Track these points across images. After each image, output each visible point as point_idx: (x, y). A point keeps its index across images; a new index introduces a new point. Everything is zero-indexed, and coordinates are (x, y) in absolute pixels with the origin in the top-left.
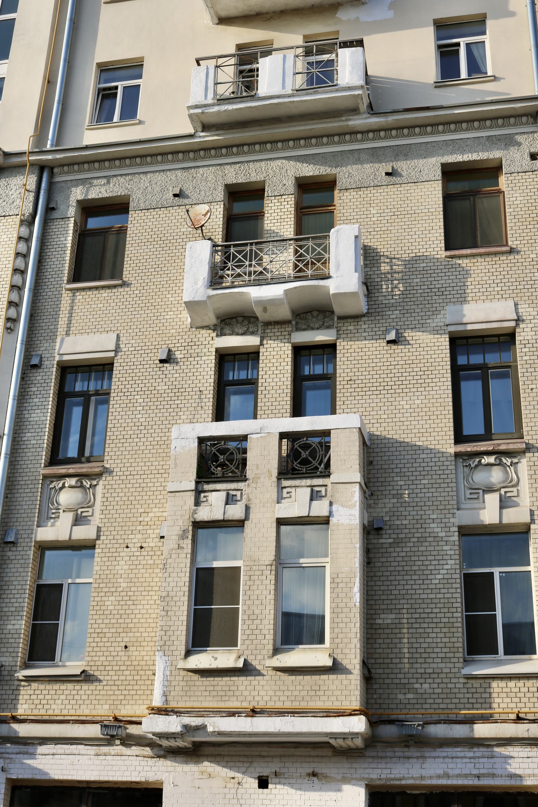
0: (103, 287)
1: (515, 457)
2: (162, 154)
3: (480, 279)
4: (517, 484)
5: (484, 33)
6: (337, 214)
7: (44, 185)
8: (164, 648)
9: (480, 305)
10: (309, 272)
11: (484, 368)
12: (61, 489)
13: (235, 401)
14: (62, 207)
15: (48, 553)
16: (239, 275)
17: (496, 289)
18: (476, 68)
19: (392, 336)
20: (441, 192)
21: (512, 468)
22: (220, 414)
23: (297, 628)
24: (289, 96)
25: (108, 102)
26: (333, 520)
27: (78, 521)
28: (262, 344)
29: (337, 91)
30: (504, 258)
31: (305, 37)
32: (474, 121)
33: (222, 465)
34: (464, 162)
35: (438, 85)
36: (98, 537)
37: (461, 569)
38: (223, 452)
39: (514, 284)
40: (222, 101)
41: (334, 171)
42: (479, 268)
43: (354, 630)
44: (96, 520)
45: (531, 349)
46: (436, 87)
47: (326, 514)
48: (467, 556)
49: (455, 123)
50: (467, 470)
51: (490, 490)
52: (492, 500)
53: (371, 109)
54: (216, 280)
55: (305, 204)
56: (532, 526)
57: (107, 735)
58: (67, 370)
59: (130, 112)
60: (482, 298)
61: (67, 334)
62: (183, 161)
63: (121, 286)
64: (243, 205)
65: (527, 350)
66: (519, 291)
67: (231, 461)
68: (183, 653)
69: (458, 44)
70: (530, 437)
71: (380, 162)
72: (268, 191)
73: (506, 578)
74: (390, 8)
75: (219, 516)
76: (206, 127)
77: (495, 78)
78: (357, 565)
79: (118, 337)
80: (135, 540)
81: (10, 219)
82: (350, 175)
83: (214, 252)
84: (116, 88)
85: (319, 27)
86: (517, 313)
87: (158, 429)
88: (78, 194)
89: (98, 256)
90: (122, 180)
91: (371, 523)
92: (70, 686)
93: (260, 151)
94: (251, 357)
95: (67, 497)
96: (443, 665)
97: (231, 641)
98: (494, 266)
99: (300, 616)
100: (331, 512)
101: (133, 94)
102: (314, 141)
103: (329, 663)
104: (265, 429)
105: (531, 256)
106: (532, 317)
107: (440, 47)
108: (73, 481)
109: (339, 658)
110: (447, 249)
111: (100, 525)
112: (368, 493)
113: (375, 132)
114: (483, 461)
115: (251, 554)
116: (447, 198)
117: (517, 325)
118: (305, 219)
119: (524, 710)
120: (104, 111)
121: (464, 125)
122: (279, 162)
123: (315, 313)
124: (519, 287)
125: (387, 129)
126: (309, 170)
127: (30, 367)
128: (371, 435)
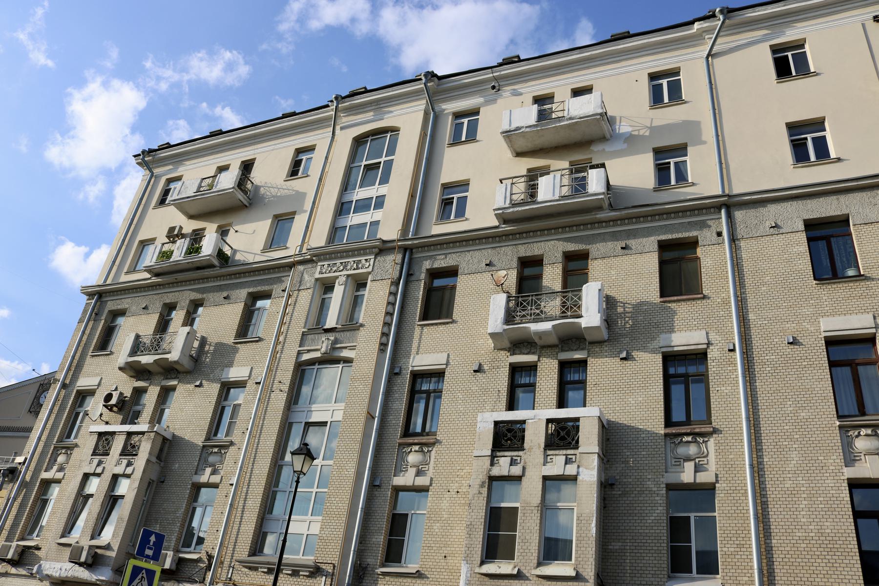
0: (440, 324)
2: (479, 239)
4: (707, 456)
6: (590, 275)
7: (406, 260)
8: (467, 559)
9: (683, 334)
10: (569, 313)
11: (686, 376)
13: (572, 395)
14: (417, 274)
15: (401, 493)
16: (524, 316)
18: (682, 177)
19: (624, 355)
22: (511, 405)
23: (554, 548)
24: (557, 200)
25: (448, 207)
26: (580, 478)
27: (419, 473)
28: (539, 360)
29: (588, 196)
31: (570, 162)
33: (510, 439)
35: (656, 190)
36: (431, 484)
37: (668, 513)
38: (509, 431)
40: (514, 205)
41: (588, 247)
42: (683, 310)
43: (591, 552)
44: (430, 473)
47: (575, 473)
48: (670, 504)
49: (667, 214)
50: (673, 445)
51: (688, 459)
52: (689, 466)
53: (611, 207)
54: (509, 318)
55: (569, 269)
56: (717, 485)
58: (417, 376)
59: (461, 213)
61: (417, 354)
62: (492, 243)
63: (451, 323)
64: (529, 271)
67: (515, 437)
68: (479, 562)
69: (669, 163)
71: (618, 240)
72: (545, 261)
73: (699, 520)
74: (624, 142)
75: (505, 473)
76: (505, 222)
77: (693, 184)
78: (595, 508)
79: (448, 355)
80: (454, 487)
81: (385, 282)
82: (598, 250)
83: (508, 301)
84: (453, 198)
85: (579, 156)
87: (469, 415)
88: (427, 265)
89: (438, 305)
90: (454, 255)
91: (607, 480)
92: (409, 580)
93: (541, 236)
94: (532, 368)
95: (413, 458)
96: (653, 579)
97: (510, 556)
99: (557, 540)
100: (578, 473)
101: (463, 201)
103: (573, 574)
104: (537, 417)
107: (792, 141)
108: (417, 448)
109: (580, 571)
110: (662, 296)
112: (605, 460)
113: (614, 221)
115: (526, 498)
116: (662, 263)
117: (708, 347)
118: (570, 278)
120: (444, 215)
121: (673, 215)
122: (552, 242)
123: (574, 340)
125: (622, 219)
126: (571, 247)
127: (394, 374)
128: (609, 421)
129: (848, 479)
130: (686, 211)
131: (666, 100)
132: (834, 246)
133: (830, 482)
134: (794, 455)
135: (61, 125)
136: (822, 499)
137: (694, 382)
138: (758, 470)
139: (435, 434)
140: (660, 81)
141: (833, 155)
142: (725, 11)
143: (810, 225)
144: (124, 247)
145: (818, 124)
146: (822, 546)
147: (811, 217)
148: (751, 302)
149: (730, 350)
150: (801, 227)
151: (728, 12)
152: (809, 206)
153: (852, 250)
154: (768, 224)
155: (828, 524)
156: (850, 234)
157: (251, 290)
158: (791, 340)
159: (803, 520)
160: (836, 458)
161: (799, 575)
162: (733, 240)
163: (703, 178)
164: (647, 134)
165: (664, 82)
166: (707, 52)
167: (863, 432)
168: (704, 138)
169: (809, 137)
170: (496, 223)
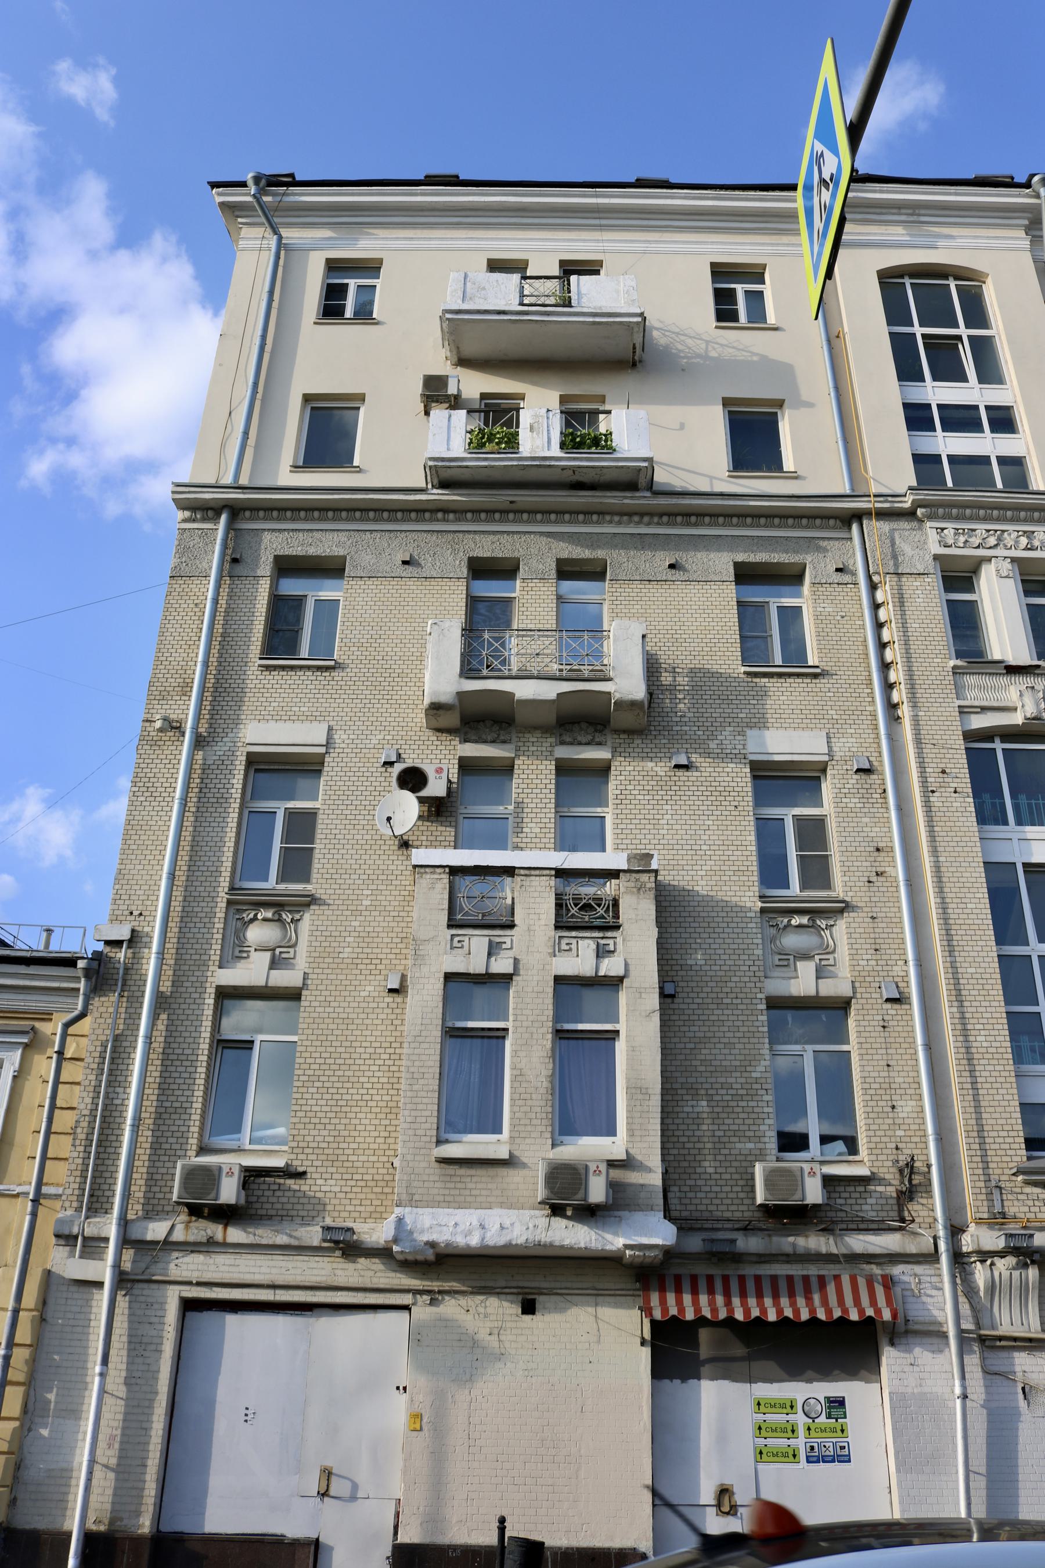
4: (294, 946)
21: (292, 926)
27: (275, 964)
32: (272, 509)
42: (783, 695)
50: (773, 931)
51: (806, 956)
52: (806, 970)
56: (304, 992)
57: (330, 1241)
86: (830, 748)
102: (385, 515)
107: (949, 602)
111: (306, 971)
114: (793, 922)
121: (721, 520)
130: (313, 510)
135: (84, 63)
142: (263, 182)
144: (258, 404)
157: (741, 557)
168: (805, 395)
170: (418, 480)
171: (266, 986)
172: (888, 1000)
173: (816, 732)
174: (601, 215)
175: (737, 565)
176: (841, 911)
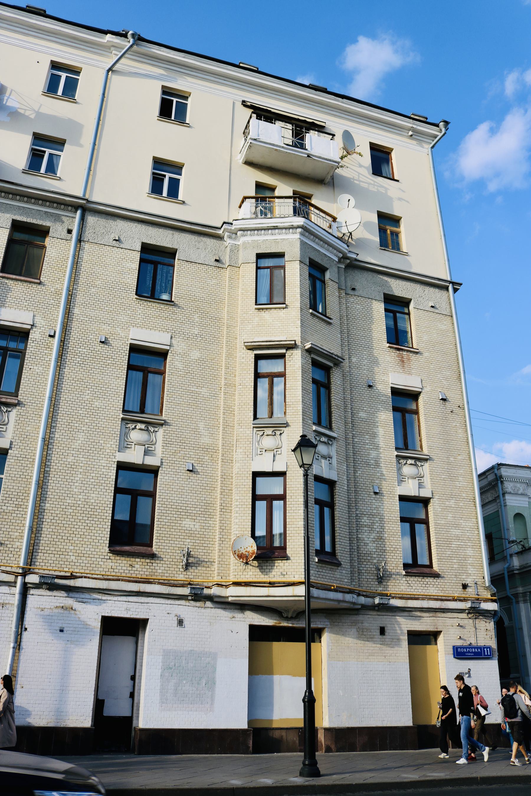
1: (10, 407)
3: (16, 295)
5: (62, 151)
12: (133, 429)
17: (25, 304)
18: (52, 169)
20: (7, 236)
27: (147, 453)
30: (34, 286)
34: (27, 222)
35: (24, 172)
39: (37, 303)
45: (36, 345)
46: (23, 172)
56: (10, 451)
60: (15, 307)
65: (34, 344)
66: (38, 308)
69: (45, 152)
70: (22, 397)
77: (60, 179)
98: (28, 290)
102: (40, 202)
105: (51, 289)
106: (42, 326)
107: (33, 149)
116: (11, 242)
119: (76, 570)
124: (39, 306)
129: (118, 462)
130: (39, 199)
131: (60, 92)
132: (159, 272)
133: (103, 462)
134: (81, 436)
136: (94, 475)
137: (11, 356)
138: (47, 443)
139: (16, 394)
140: (60, 73)
141: (180, 197)
142: (136, 37)
143: (146, 248)
145: (177, 168)
146: (85, 512)
147: (149, 242)
148: (79, 299)
149: (50, 336)
150: (139, 248)
151: (139, 39)
152: (150, 232)
153: (171, 279)
154: (112, 236)
155: (94, 495)
156: (173, 266)
158: (103, 340)
159: (75, 490)
160: (113, 443)
161: (61, 534)
162: (80, 240)
163: (69, 178)
164: (32, 117)
165: (64, 76)
166: (109, 66)
167: (139, 426)
168: (82, 142)
169: (168, 175)
171: (143, 464)
172: (188, 470)
173: (166, 333)
174: (57, 36)
175: (14, 221)
176: (162, 425)
